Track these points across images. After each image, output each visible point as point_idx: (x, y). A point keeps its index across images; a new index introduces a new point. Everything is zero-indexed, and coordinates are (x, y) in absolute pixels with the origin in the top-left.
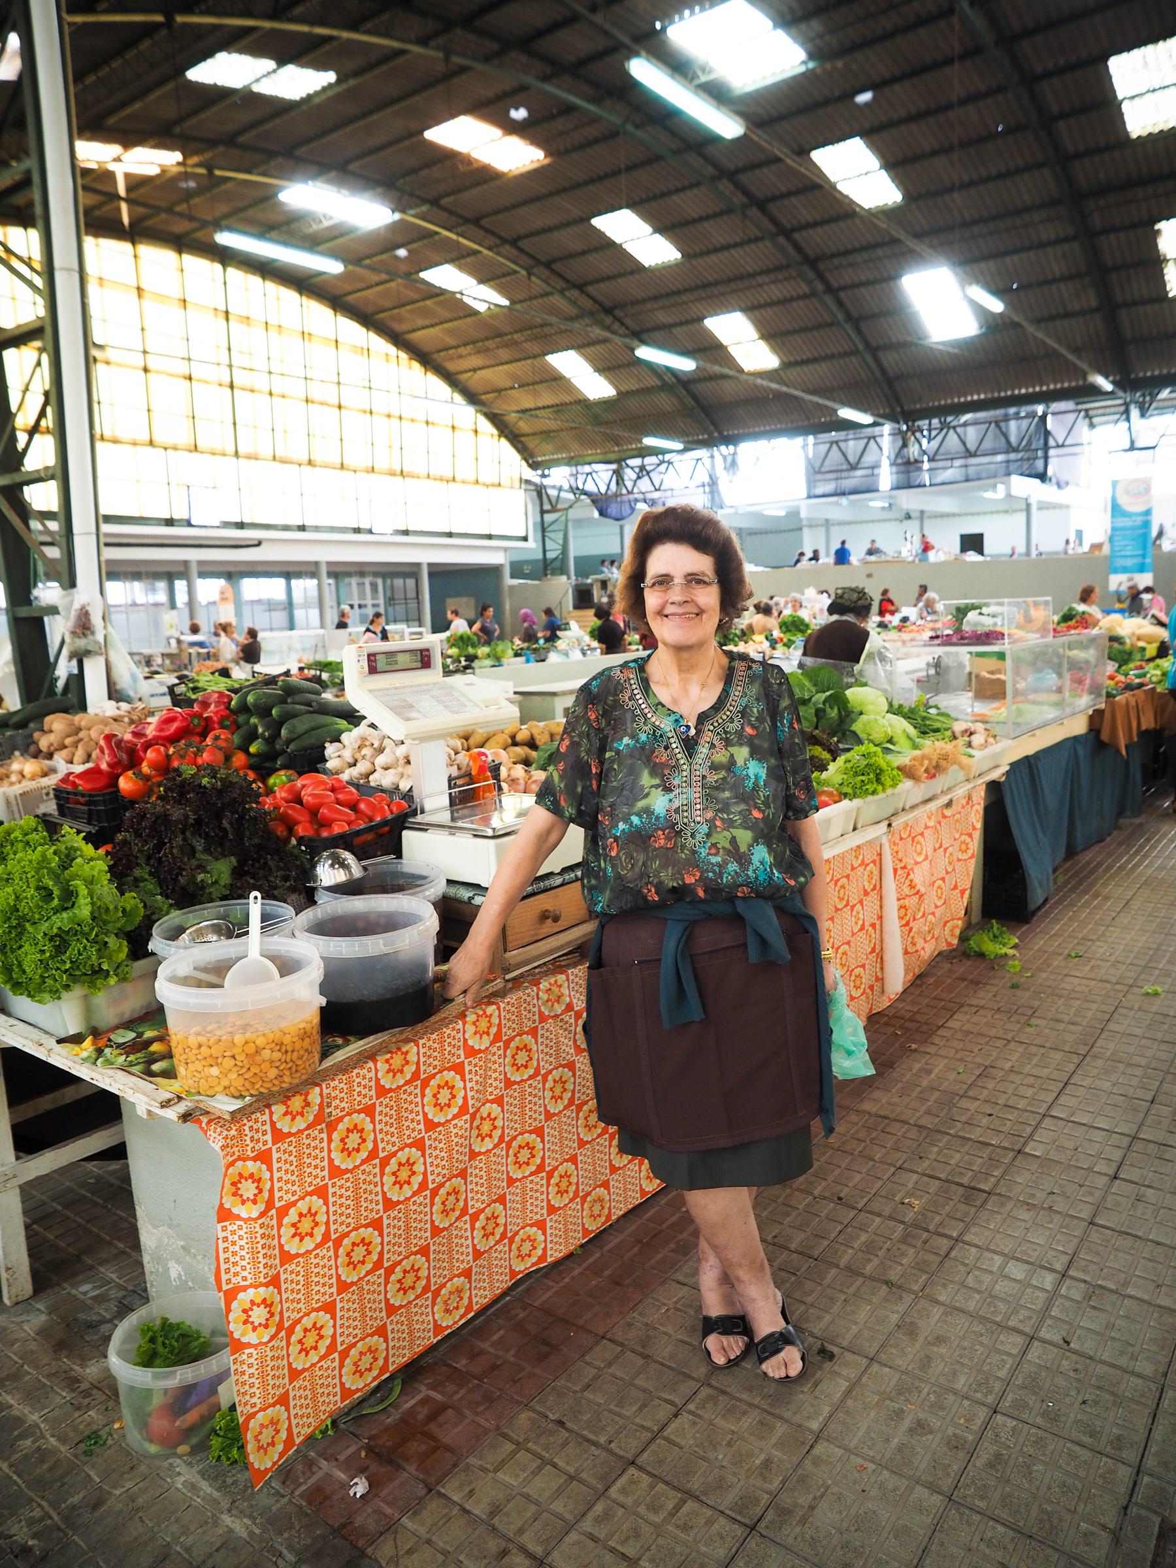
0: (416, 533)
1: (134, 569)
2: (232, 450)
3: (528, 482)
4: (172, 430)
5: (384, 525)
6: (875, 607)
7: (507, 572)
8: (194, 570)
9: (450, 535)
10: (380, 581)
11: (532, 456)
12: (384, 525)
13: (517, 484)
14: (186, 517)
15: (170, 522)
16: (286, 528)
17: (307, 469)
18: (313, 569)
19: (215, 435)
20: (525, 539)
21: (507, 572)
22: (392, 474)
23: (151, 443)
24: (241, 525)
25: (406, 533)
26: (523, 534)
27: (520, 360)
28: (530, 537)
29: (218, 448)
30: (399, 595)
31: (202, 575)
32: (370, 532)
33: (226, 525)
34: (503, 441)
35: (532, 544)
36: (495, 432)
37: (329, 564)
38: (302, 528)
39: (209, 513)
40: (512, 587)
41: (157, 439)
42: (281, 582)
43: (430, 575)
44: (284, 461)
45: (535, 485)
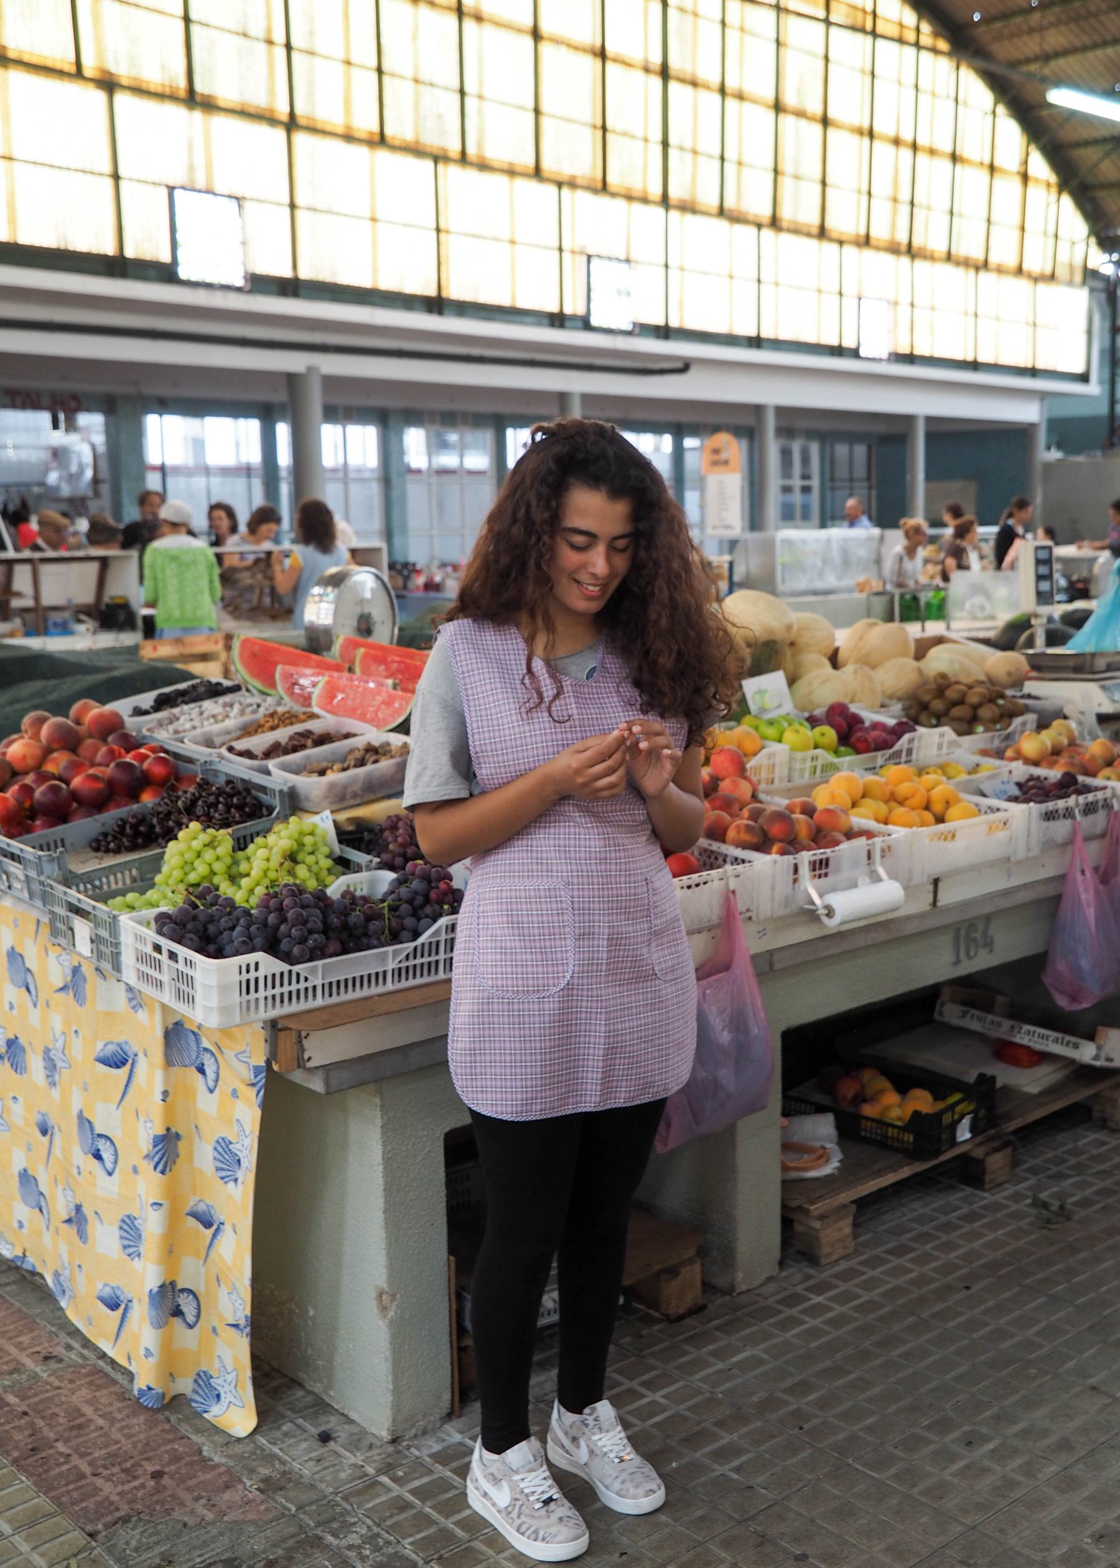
0: (777, 345)
1: (377, 402)
2: (656, 191)
3: (1090, 275)
4: (568, 151)
5: (876, 346)
6: (87, 970)
7: (1042, 437)
8: (315, 401)
9: (974, 366)
10: (814, 449)
11: (1109, 225)
12: (876, 346)
13: (1078, 277)
14: (581, 311)
15: (558, 320)
16: (730, 340)
17: (767, 234)
18: (749, 421)
19: (633, 165)
20: (1084, 378)
21: (1042, 437)
22: (893, 249)
23: (537, 173)
24: (664, 332)
25: (910, 359)
26: (1079, 368)
27: (1085, 48)
28: (1094, 376)
29: (637, 186)
30: (842, 472)
31: (332, 414)
32: (585, 324)
33: (259, 284)
34: (1067, 201)
35: (1094, 388)
36: (1053, 178)
37: (930, 420)
38: (756, 342)
39: (216, 254)
40: (1048, 466)
41: (548, 165)
42: (252, 427)
43: (930, 437)
44: (483, 166)
45: (1106, 279)
